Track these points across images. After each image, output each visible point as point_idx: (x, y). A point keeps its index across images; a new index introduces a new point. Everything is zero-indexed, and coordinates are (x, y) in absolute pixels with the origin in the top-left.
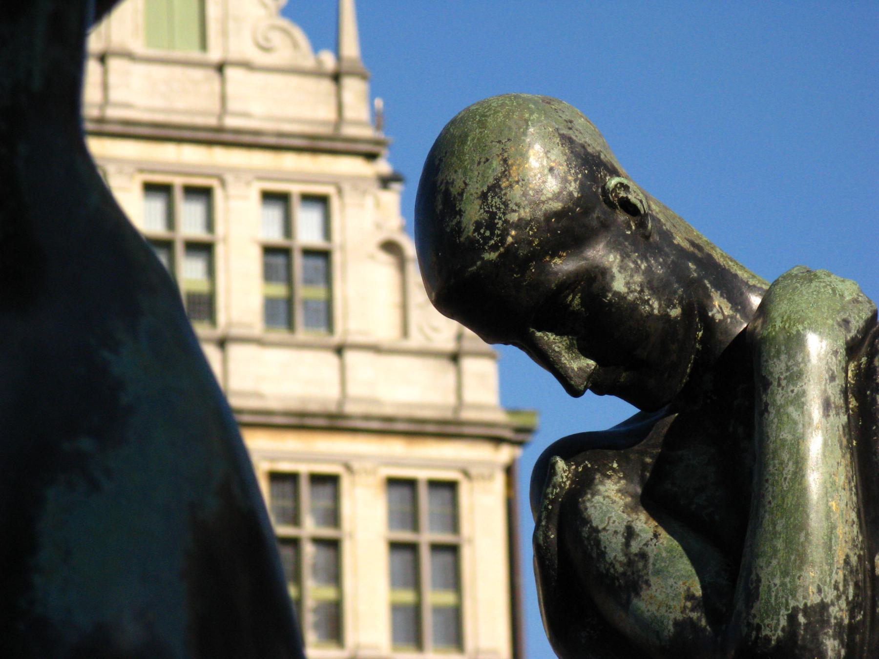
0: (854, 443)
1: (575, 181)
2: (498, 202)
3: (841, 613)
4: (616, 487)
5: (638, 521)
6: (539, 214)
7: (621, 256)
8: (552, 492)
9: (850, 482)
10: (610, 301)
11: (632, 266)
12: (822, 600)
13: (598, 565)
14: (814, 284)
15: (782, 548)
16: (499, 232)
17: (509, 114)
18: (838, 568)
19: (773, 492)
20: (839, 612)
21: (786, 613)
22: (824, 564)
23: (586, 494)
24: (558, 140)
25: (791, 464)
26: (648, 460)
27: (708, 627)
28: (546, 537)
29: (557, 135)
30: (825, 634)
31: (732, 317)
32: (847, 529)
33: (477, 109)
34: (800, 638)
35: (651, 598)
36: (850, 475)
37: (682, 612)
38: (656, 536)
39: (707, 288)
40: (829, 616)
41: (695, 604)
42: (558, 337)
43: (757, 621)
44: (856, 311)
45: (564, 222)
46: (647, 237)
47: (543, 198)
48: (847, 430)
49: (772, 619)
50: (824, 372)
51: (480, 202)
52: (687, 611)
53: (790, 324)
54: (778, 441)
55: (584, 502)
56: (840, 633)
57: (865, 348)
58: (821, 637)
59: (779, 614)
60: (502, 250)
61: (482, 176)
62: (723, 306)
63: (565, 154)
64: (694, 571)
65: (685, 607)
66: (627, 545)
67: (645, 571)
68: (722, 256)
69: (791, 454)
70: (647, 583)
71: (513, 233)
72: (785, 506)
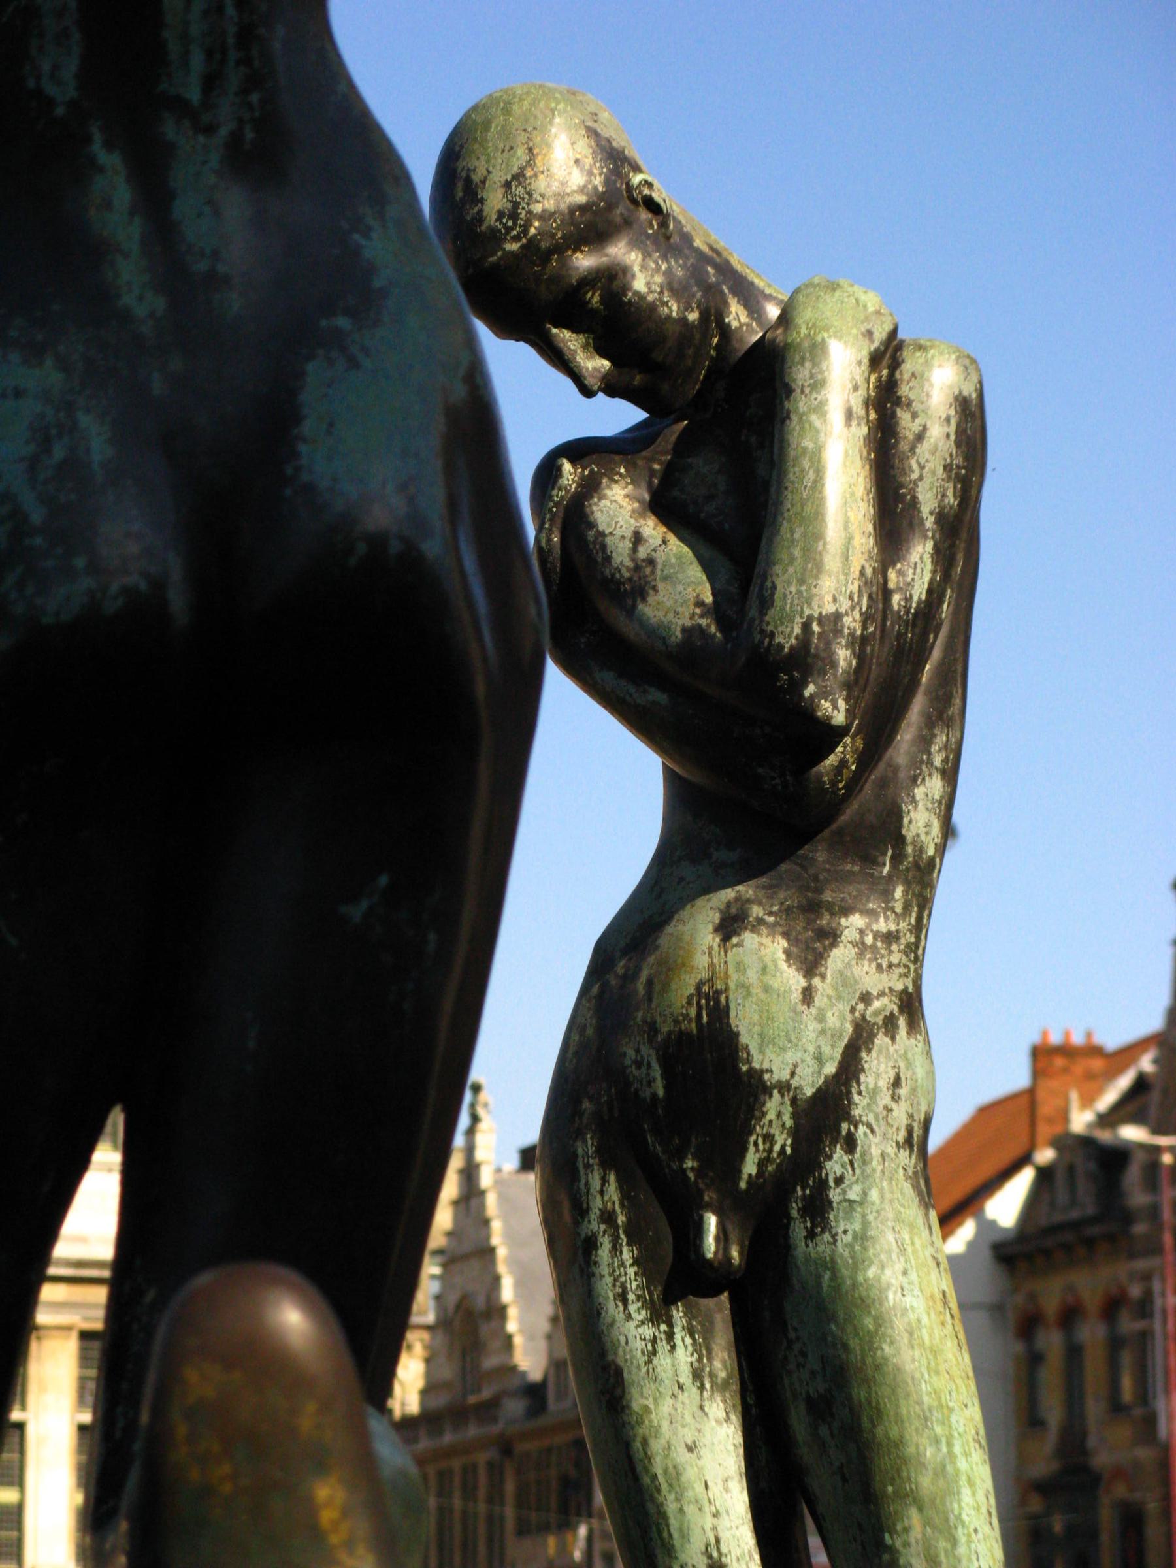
0: (872, 456)
1: (600, 174)
2: (522, 192)
3: (854, 624)
4: (623, 492)
5: (645, 527)
6: (563, 207)
7: (643, 254)
8: (557, 495)
9: (868, 494)
10: (630, 301)
11: (653, 265)
12: (837, 610)
13: (603, 570)
14: (837, 293)
15: (799, 556)
16: (522, 223)
17: (534, 103)
18: (854, 579)
19: (793, 499)
20: (852, 622)
21: (801, 621)
22: (841, 573)
23: (592, 497)
24: (584, 132)
25: (811, 472)
26: (656, 467)
27: (718, 635)
28: (549, 540)
29: (583, 127)
30: (838, 643)
31: (748, 325)
32: (864, 540)
33: (501, 96)
34: (813, 646)
35: (658, 603)
36: (868, 486)
37: (690, 619)
38: (664, 542)
39: (725, 294)
40: (843, 626)
41: (705, 611)
42: (574, 335)
43: (770, 628)
44: (879, 323)
45: (588, 216)
46: (668, 238)
47: (568, 190)
48: (867, 442)
49: (787, 627)
50: (848, 382)
51: (503, 190)
52: (696, 617)
53: (815, 331)
54: (799, 449)
55: (590, 505)
56: (852, 643)
57: (886, 361)
58: (834, 646)
59: (794, 622)
60: (524, 241)
61: (507, 164)
62: (739, 313)
63: (591, 147)
64: (704, 578)
65: (694, 614)
66: (635, 550)
67: (653, 577)
68: (739, 261)
69: (811, 460)
70: (655, 588)
71: (536, 224)
72: (804, 515)
